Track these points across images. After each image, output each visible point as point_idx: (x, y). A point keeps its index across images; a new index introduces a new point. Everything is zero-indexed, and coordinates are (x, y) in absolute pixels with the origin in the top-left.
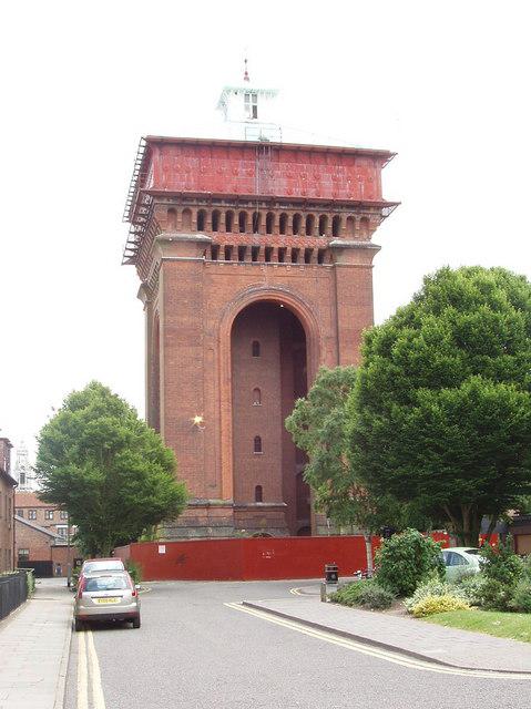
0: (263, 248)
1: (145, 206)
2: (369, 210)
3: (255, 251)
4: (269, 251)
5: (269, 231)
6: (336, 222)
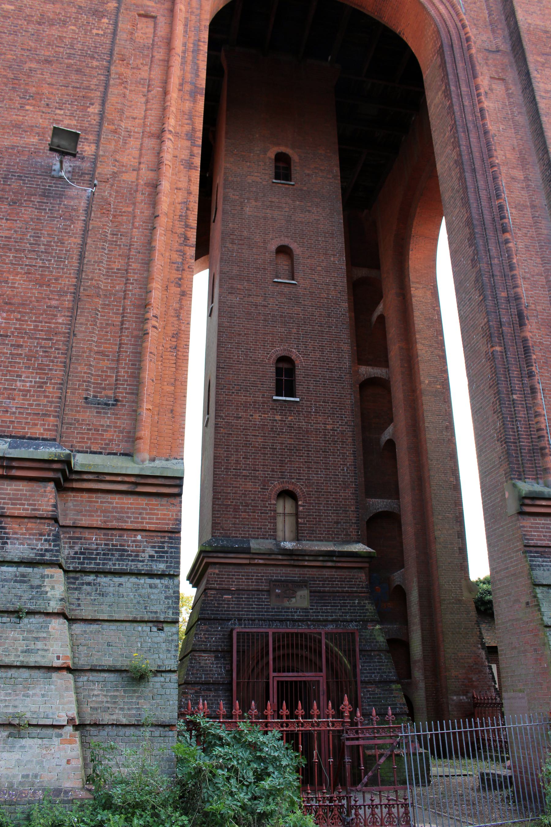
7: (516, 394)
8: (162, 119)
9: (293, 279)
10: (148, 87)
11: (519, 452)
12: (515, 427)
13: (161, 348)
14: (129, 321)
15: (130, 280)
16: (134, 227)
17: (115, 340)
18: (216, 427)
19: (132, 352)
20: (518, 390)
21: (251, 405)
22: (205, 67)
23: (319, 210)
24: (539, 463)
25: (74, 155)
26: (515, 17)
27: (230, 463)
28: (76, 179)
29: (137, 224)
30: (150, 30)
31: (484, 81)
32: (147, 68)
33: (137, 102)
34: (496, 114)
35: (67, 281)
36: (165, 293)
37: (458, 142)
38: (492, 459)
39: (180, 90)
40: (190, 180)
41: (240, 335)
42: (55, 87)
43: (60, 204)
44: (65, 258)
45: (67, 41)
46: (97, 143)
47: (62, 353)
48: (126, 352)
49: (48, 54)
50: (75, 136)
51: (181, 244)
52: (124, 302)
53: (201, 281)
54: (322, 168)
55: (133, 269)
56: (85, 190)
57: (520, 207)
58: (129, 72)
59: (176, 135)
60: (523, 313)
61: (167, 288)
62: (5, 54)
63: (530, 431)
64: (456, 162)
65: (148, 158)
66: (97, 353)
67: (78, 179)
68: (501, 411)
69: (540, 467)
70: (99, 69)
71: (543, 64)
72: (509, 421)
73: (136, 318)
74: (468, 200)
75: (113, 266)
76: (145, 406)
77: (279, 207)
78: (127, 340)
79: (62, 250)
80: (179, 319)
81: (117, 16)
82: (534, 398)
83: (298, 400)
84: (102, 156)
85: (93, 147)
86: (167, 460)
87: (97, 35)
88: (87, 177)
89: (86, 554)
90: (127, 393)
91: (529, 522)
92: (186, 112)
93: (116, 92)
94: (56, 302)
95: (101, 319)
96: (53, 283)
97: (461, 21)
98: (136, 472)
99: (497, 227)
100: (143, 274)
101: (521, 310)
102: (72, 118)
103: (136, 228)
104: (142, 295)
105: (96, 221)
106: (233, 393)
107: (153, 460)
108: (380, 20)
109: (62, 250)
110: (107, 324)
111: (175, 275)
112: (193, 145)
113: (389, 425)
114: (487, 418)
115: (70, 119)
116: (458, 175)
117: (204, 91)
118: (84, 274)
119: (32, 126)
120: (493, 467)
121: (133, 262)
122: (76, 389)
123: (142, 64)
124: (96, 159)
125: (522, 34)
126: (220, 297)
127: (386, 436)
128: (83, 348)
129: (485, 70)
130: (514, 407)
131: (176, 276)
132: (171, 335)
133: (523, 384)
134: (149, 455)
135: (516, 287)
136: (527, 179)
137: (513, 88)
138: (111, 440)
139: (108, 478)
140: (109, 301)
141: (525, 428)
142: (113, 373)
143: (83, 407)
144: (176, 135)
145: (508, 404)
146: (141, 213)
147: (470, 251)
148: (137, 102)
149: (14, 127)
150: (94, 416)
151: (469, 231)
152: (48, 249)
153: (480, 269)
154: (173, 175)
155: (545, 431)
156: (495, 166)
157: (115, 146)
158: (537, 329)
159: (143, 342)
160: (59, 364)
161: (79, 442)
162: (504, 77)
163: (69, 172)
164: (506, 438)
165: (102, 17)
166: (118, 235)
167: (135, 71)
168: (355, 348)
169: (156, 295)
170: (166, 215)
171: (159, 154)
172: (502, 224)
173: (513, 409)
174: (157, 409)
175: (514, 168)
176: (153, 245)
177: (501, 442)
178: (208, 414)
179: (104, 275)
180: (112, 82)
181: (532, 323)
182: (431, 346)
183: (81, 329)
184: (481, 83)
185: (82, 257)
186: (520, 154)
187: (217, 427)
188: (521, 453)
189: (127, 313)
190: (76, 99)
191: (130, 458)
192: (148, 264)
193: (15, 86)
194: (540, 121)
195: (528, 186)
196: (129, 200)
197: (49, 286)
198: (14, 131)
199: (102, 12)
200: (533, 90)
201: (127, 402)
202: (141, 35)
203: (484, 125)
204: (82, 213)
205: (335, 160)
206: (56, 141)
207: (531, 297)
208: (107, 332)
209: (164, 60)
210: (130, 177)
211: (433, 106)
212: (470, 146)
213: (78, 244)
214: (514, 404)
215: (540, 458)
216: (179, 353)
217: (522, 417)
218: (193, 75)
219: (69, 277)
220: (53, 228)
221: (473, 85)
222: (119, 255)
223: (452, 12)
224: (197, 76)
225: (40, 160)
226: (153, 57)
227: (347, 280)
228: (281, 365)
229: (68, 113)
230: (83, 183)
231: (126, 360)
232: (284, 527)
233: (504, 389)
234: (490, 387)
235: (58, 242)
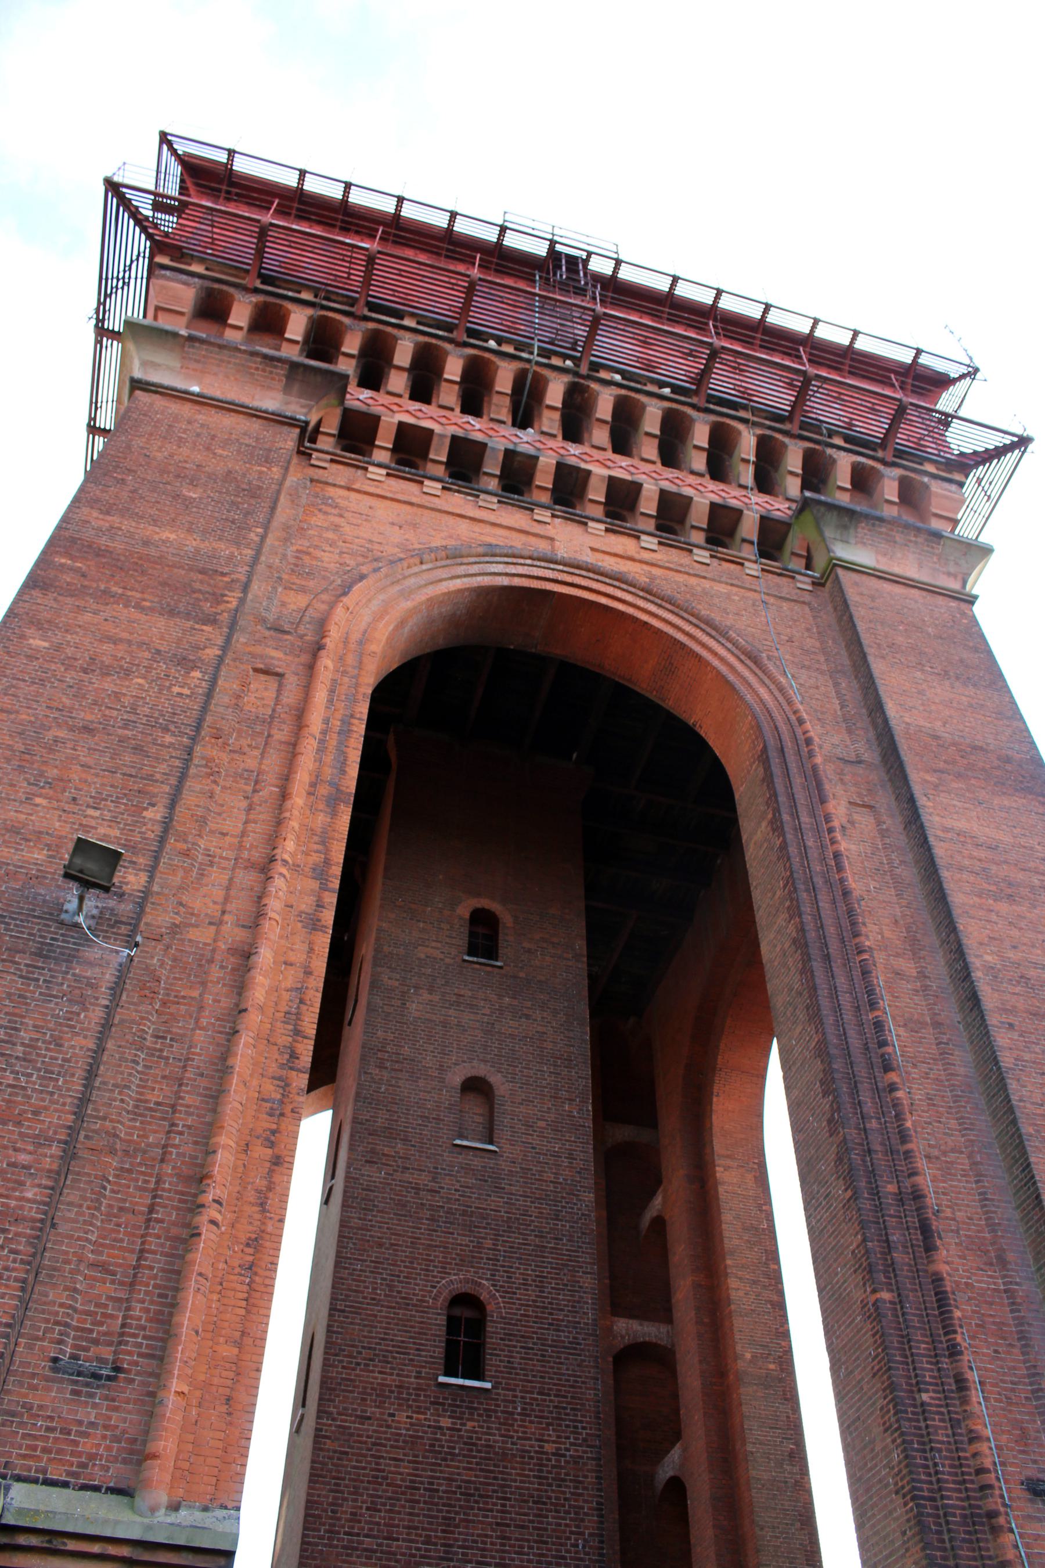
7: (927, 1391)
8: (274, 839)
9: (491, 1143)
10: (255, 785)
11: (942, 1521)
12: (930, 1463)
13: (221, 1266)
14: (165, 1206)
15: (177, 1125)
16: (198, 1026)
17: (133, 1243)
18: (316, 1436)
19: (163, 1270)
20: (930, 1384)
21: (392, 1392)
22: (359, 760)
23: (545, 1014)
24: (988, 1549)
25: (107, 889)
26: (883, 712)
27: (339, 1519)
28: (102, 931)
29: (204, 1022)
30: (271, 694)
31: (838, 809)
32: (256, 753)
33: (233, 807)
34: (862, 863)
35: (56, 1119)
36: (243, 1156)
37: (798, 907)
38: (888, 1535)
39: (309, 794)
40: (311, 950)
41: (381, 1245)
42: (93, 771)
43: (67, 973)
44: (59, 1074)
45: (126, 701)
46: (152, 871)
47: (22, 1261)
48: (151, 1268)
49: (90, 717)
50: (113, 858)
51: (282, 1066)
52: (160, 1168)
53: (314, 1132)
54: (555, 940)
55: (188, 1106)
56: (117, 952)
57: (912, 1025)
58: (225, 757)
59: (295, 868)
60: (930, 1225)
61: (247, 1148)
62: (17, 712)
63: (963, 1474)
64: (794, 941)
65: (241, 904)
66: (93, 1265)
67: (107, 931)
68: (899, 1428)
69: (990, 1558)
70: (175, 749)
71: (936, 787)
72: (917, 1450)
73: (180, 1201)
74: (819, 1010)
75: (148, 1097)
77: (471, 1006)
78: (157, 1244)
79: (56, 1059)
80: (264, 1211)
81: (218, 669)
82: (965, 1401)
83: (488, 1385)
84: (158, 893)
85: (143, 878)
86: (206, 1509)
87: (180, 694)
88: (124, 929)
90: (140, 1355)
92: (316, 831)
93: (198, 787)
94: (28, 1157)
95: (111, 1198)
96: (28, 1120)
97: (795, 712)
98: (135, 1534)
99: (874, 1060)
100: (204, 1116)
101: (927, 1219)
102: (113, 824)
103: (201, 1029)
104: (196, 1158)
105: (128, 1009)
106: (358, 1364)
107: (175, 1507)
108: (660, 703)
109: (56, 1059)
110: (121, 1209)
111: (266, 1123)
112: (324, 887)
113: (673, 1444)
114: (872, 1441)
115: (110, 826)
116: (800, 965)
117: (352, 799)
118: (90, 1106)
119: (40, 833)
120: (890, 1555)
121: (187, 1092)
122: (37, 1338)
123: (249, 746)
124: (145, 899)
125: (897, 738)
126: (348, 1167)
127: (666, 1470)
128: (66, 1253)
129: (839, 790)
130: (925, 1420)
131: (267, 1125)
132: (244, 1240)
133: (939, 1370)
134: (169, 1495)
135: (913, 1173)
136: (922, 975)
137: (889, 822)
138: (92, 1457)
139: (72, 1545)
140: (131, 1164)
141: (951, 1466)
142: (120, 1310)
143: (47, 1379)
144: (295, 868)
145: (913, 1413)
146: (215, 1001)
147: (826, 1103)
148: (233, 807)
149: (7, 830)
150: (65, 1399)
151: (821, 1067)
152: (30, 1053)
153: (845, 1138)
154: (281, 937)
155: (993, 1475)
156: (865, 951)
157: (182, 878)
158: (960, 1257)
159: (187, 1251)
160: (11, 1283)
161: (24, 1457)
162: (872, 803)
163: (93, 917)
164: (914, 1488)
165: (192, 669)
166: (165, 1038)
167: (236, 756)
168: (607, 1281)
169: (224, 1160)
170: (261, 1008)
171: (260, 899)
172: (883, 1055)
173: (922, 1424)
174: (198, 1393)
175: (897, 955)
176: (230, 1062)
177: (904, 1496)
178: (304, 1405)
179: (128, 1112)
180: (193, 771)
181: (949, 1244)
182: (755, 1282)
183: (68, 1215)
184: (833, 811)
185: (91, 1074)
186: (908, 932)
187: (319, 1436)
188: (947, 1523)
189: (164, 1190)
190: (125, 795)
191: (125, 1500)
192: (217, 1097)
193: (24, 764)
194: (939, 877)
195: (925, 988)
196: (196, 976)
197: (19, 1124)
198: (7, 837)
199: (193, 661)
200: (922, 826)
201: (138, 1373)
202: (253, 699)
203: (842, 881)
204: (104, 993)
205: (579, 928)
206: (78, 861)
207: (944, 1194)
208: (119, 1225)
209: (288, 743)
210: (202, 935)
211: (752, 845)
212: (818, 916)
213: (89, 1050)
214: (924, 1412)
215: (989, 1537)
216: (257, 1279)
217: (942, 1442)
218: (335, 771)
219: (61, 1111)
220: (46, 1015)
221: (820, 812)
222: (164, 1077)
223: (781, 699)
224: (343, 772)
225: (43, 892)
226: (269, 736)
227: (594, 1149)
228: (457, 1312)
229: (108, 815)
230: (116, 940)
231: (147, 1285)
233: (903, 1381)
234: (874, 1375)
235: (50, 1043)
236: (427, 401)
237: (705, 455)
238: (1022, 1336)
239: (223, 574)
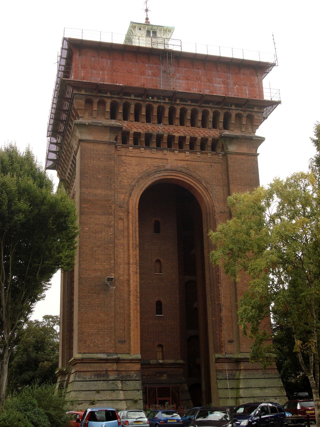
0: (166, 135)
1: (64, 111)
2: (258, 108)
3: (159, 138)
4: (171, 138)
5: (171, 123)
6: (227, 117)
8: (129, 259)
45: (103, 238)
65: (126, 272)
76: (132, 343)
89: (123, 377)
91: (217, 364)
232: (159, 355)
236: (138, 121)
237: (201, 122)
238: (232, 322)
239: (110, 200)
